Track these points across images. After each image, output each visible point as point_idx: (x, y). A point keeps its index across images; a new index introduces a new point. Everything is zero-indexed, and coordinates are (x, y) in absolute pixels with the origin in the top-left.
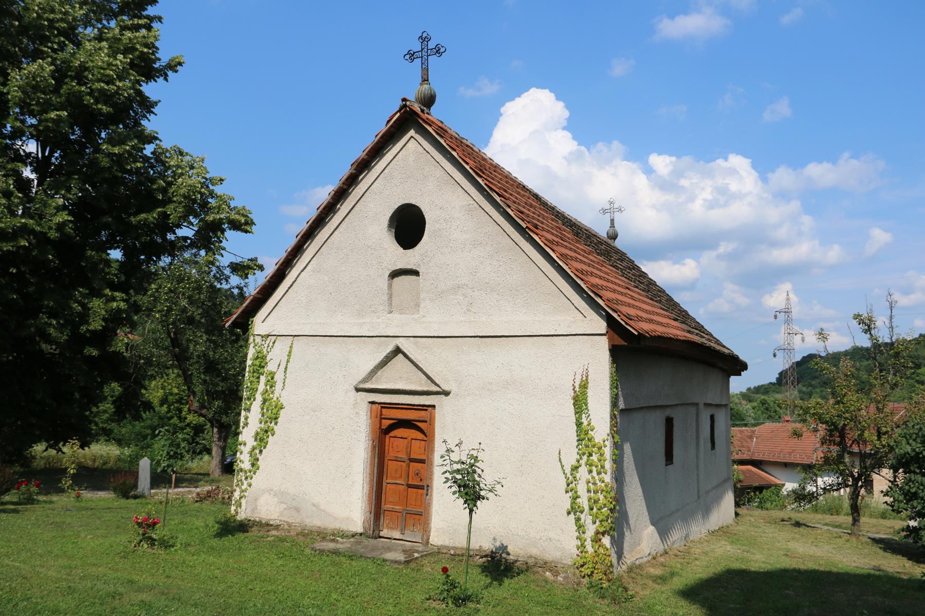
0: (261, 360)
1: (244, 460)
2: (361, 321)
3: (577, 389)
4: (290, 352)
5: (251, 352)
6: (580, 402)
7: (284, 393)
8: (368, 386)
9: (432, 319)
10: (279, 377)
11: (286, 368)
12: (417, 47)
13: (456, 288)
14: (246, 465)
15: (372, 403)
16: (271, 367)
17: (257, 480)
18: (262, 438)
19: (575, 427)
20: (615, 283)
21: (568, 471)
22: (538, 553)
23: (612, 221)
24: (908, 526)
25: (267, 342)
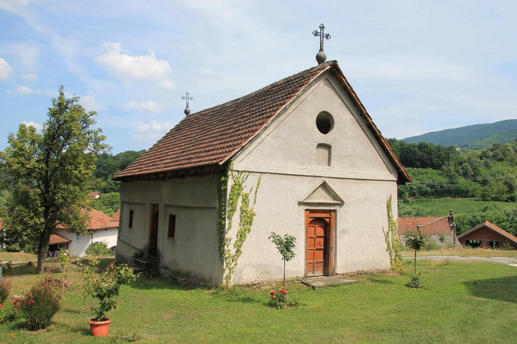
0: (238, 186)
1: (230, 248)
5: (230, 183)
6: (389, 207)
9: (337, 169)
10: (251, 197)
14: (233, 252)
15: (306, 210)
16: (245, 191)
17: (240, 260)
18: (242, 236)
21: (386, 234)
23: (187, 104)
25: (242, 175)
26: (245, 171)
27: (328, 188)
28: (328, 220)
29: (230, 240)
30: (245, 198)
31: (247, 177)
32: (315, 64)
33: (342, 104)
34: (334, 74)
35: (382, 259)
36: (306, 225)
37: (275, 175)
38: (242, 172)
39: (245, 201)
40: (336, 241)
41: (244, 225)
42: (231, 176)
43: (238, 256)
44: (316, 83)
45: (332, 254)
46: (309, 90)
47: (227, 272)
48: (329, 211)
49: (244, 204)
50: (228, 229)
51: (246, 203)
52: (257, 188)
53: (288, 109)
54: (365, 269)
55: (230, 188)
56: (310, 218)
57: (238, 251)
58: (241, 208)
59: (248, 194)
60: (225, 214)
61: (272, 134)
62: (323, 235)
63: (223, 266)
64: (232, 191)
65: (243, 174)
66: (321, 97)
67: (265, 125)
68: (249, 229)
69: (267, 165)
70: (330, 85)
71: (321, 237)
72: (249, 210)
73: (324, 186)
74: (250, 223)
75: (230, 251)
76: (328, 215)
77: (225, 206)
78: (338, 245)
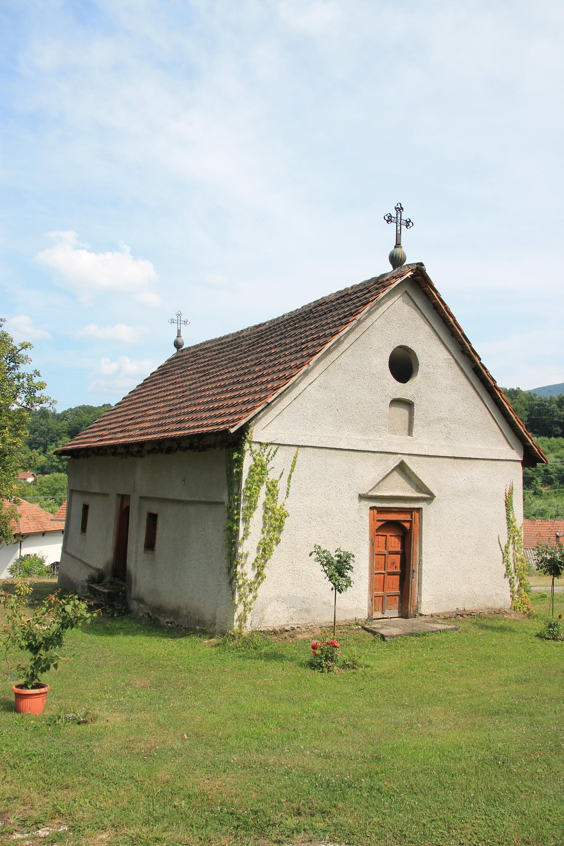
0: (260, 468)
1: (246, 570)
5: (248, 462)
6: (508, 505)
7: (287, 501)
9: (423, 441)
10: (282, 485)
12: (405, 216)
13: (440, 420)
14: (251, 576)
15: (372, 508)
16: (272, 476)
17: (262, 590)
18: (265, 550)
20: (147, 391)
21: (503, 549)
23: (179, 331)
25: (267, 450)
26: (272, 444)
27: (407, 472)
28: (407, 525)
29: (247, 556)
30: (271, 488)
31: (275, 453)
32: (388, 268)
33: (432, 333)
34: (419, 283)
36: (371, 532)
37: (322, 450)
38: (267, 445)
39: (272, 492)
40: (420, 560)
41: (268, 532)
42: (249, 452)
43: (259, 584)
45: (414, 581)
46: (377, 312)
47: (240, 609)
48: (410, 511)
49: (270, 497)
50: (243, 539)
51: (273, 496)
52: (292, 471)
53: (343, 342)
54: (469, 607)
55: (248, 471)
57: (259, 574)
58: (265, 504)
59: (276, 482)
60: (238, 514)
61: (316, 382)
62: (399, 549)
65: (269, 448)
66: (397, 322)
68: (277, 538)
72: (278, 507)
73: (402, 468)
74: (280, 529)
75: (245, 575)
76: (407, 517)
77: (239, 500)
78: (424, 567)
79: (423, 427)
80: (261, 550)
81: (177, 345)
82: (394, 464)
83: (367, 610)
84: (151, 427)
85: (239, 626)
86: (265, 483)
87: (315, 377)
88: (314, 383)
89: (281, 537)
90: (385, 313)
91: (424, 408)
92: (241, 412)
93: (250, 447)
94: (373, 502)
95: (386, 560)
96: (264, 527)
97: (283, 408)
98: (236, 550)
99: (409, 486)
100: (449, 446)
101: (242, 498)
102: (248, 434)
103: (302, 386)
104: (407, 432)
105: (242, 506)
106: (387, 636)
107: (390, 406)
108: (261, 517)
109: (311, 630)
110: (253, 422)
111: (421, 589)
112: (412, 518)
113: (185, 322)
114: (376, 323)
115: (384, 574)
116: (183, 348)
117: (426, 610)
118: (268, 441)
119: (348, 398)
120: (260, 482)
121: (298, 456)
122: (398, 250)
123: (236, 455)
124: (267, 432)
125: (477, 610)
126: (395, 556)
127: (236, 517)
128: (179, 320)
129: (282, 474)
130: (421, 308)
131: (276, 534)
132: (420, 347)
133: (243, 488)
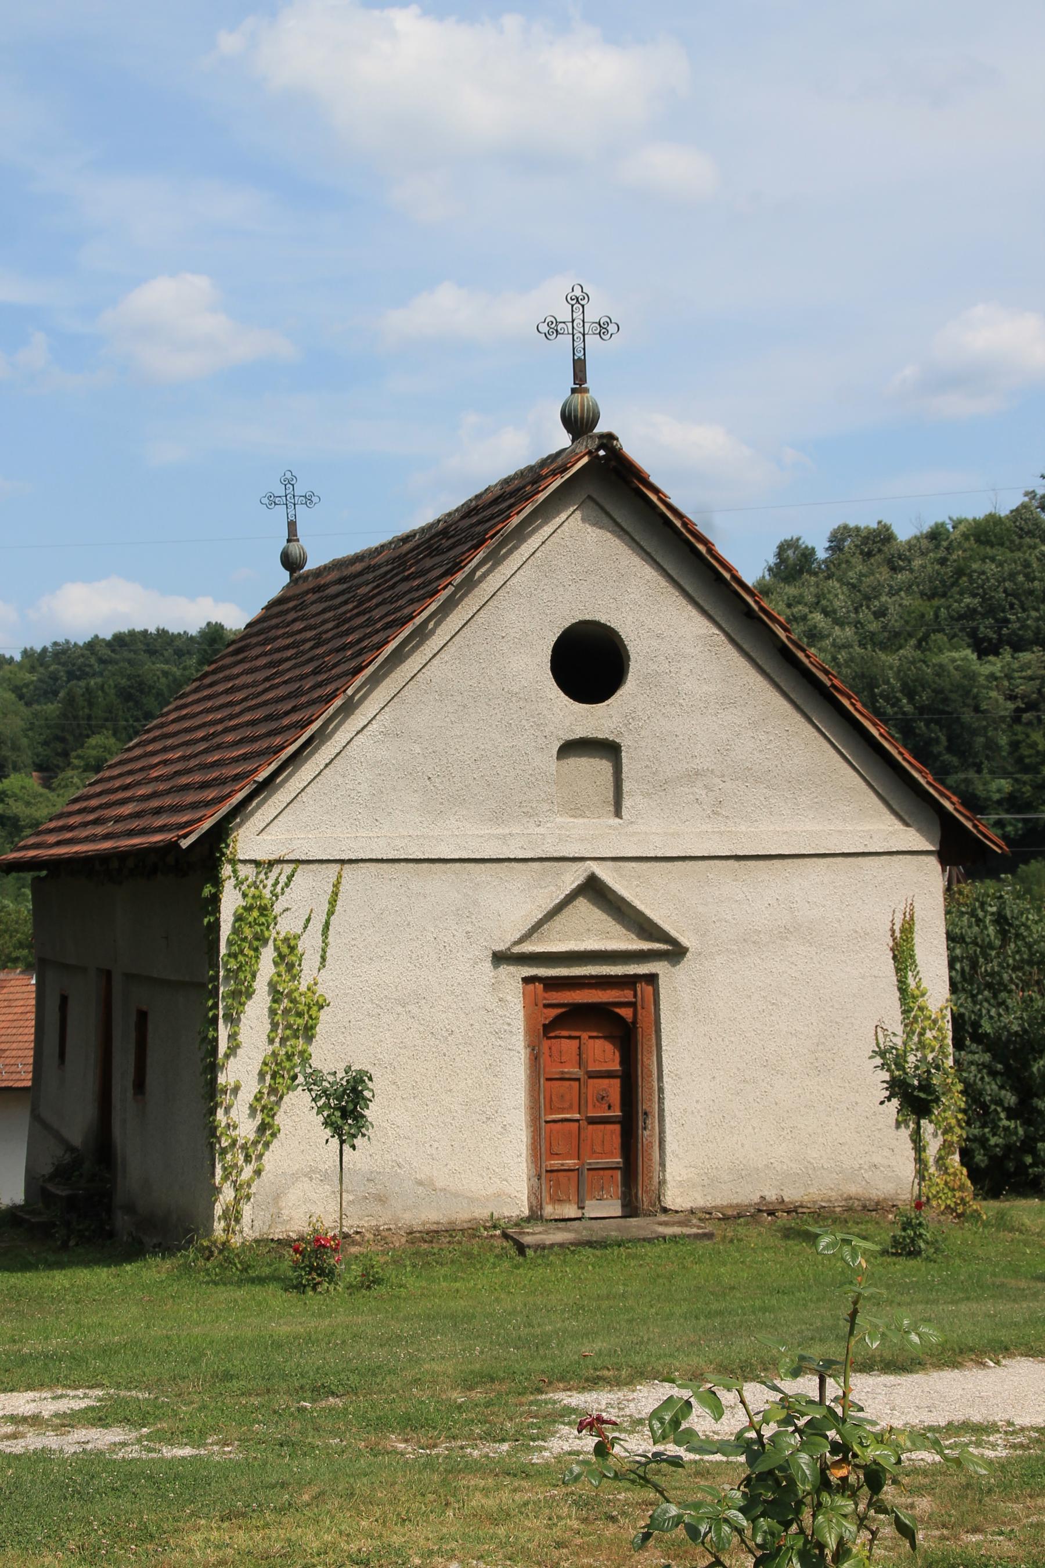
0: (258, 914)
2: (500, 831)
3: (898, 934)
4: (335, 894)
5: (230, 902)
6: (902, 956)
8: (528, 948)
9: (646, 828)
10: (309, 945)
11: (327, 926)
14: (246, 1129)
15: (527, 980)
16: (286, 926)
17: (274, 1159)
19: (898, 994)
22: (860, 1191)
23: (292, 526)
24: (982, 1455)
25: (273, 875)
26: (280, 861)
27: (610, 897)
28: (626, 1013)
29: (236, 1089)
30: (285, 950)
31: (290, 878)
32: (563, 440)
33: (663, 583)
34: (607, 480)
35: (877, 1159)
36: (530, 1031)
37: (396, 865)
38: (271, 864)
39: (288, 957)
40: (661, 1090)
41: (283, 1041)
42: (233, 881)
43: (267, 1145)
44: (546, 522)
45: (648, 1135)
46: (516, 555)
47: (227, 1194)
48: (630, 982)
49: (282, 968)
50: (227, 1056)
51: (290, 967)
52: (331, 913)
53: (432, 632)
54: (792, 1194)
55: (232, 919)
56: (546, 1006)
57: (262, 1128)
58: (273, 986)
59: (297, 937)
60: (216, 1006)
61: (375, 725)
62: (616, 1067)
63: (213, 1175)
64: (235, 931)
65: (276, 870)
66: (575, 570)
67: (338, 702)
68: (302, 1053)
69: (362, 833)
70: (606, 520)
71: (609, 1075)
72: (303, 988)
73: (594, 889)
74: (308, 1033)
75: (235, 1127)
76: (626, 995)
77: (216, 977)
78: (668, 1105)
79: (648, 795)
80: (268, 1077)
81: (290, 562)
82: (573, 882)
83: (525, 1198)
84: (85, 825)
85: (224, 1230)
86: (271, 943)
87: (370, 716)
88: (368, 728)
89: (311, 1049)
90: (537, 555)
91: (649, 752)
92: (194, 806)
93: (235, 871)
94: (530, 966)
95: (583, 1090)
96: (272, 1031)
97: (302, 786)
98: (215, 1079)
99: (618, 927)
100: (721, 833)
101: (222, 973)
102: (227, 846)
103: (341, 737)
104: (612, 808)
105: (221, 990)
106: (529, 1247)
107: (558, 758)
108: (266, 1012)
109: (384, 1238)
110: (238, 820)
111: (664, 1152)
112: (635, 996)
113: (308, 500)
114: (514, 580)
115: (578, 1121)
116: (306, 568)
117: (679, 1200)
118: (272, 857)
119: (453, 751)
120: (258, 939)
121: (343, 881)
122: (578, 397)
123: (208, 890)
124: (269, 837)
125: (815, 1202)
126: (606, 1081)
127: (211, 1014)
128: (290, 497)
129: (308, 920)
130: (629, 530)
131: (301, 1044)
132: (630, 618)
133: (221, 955)
